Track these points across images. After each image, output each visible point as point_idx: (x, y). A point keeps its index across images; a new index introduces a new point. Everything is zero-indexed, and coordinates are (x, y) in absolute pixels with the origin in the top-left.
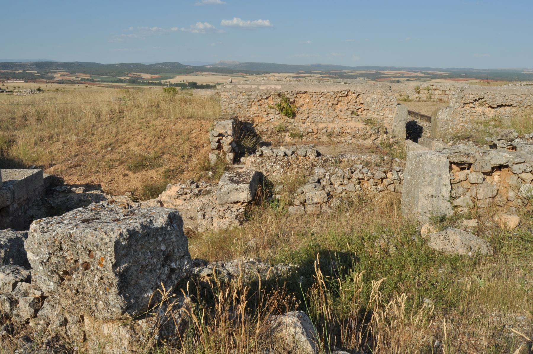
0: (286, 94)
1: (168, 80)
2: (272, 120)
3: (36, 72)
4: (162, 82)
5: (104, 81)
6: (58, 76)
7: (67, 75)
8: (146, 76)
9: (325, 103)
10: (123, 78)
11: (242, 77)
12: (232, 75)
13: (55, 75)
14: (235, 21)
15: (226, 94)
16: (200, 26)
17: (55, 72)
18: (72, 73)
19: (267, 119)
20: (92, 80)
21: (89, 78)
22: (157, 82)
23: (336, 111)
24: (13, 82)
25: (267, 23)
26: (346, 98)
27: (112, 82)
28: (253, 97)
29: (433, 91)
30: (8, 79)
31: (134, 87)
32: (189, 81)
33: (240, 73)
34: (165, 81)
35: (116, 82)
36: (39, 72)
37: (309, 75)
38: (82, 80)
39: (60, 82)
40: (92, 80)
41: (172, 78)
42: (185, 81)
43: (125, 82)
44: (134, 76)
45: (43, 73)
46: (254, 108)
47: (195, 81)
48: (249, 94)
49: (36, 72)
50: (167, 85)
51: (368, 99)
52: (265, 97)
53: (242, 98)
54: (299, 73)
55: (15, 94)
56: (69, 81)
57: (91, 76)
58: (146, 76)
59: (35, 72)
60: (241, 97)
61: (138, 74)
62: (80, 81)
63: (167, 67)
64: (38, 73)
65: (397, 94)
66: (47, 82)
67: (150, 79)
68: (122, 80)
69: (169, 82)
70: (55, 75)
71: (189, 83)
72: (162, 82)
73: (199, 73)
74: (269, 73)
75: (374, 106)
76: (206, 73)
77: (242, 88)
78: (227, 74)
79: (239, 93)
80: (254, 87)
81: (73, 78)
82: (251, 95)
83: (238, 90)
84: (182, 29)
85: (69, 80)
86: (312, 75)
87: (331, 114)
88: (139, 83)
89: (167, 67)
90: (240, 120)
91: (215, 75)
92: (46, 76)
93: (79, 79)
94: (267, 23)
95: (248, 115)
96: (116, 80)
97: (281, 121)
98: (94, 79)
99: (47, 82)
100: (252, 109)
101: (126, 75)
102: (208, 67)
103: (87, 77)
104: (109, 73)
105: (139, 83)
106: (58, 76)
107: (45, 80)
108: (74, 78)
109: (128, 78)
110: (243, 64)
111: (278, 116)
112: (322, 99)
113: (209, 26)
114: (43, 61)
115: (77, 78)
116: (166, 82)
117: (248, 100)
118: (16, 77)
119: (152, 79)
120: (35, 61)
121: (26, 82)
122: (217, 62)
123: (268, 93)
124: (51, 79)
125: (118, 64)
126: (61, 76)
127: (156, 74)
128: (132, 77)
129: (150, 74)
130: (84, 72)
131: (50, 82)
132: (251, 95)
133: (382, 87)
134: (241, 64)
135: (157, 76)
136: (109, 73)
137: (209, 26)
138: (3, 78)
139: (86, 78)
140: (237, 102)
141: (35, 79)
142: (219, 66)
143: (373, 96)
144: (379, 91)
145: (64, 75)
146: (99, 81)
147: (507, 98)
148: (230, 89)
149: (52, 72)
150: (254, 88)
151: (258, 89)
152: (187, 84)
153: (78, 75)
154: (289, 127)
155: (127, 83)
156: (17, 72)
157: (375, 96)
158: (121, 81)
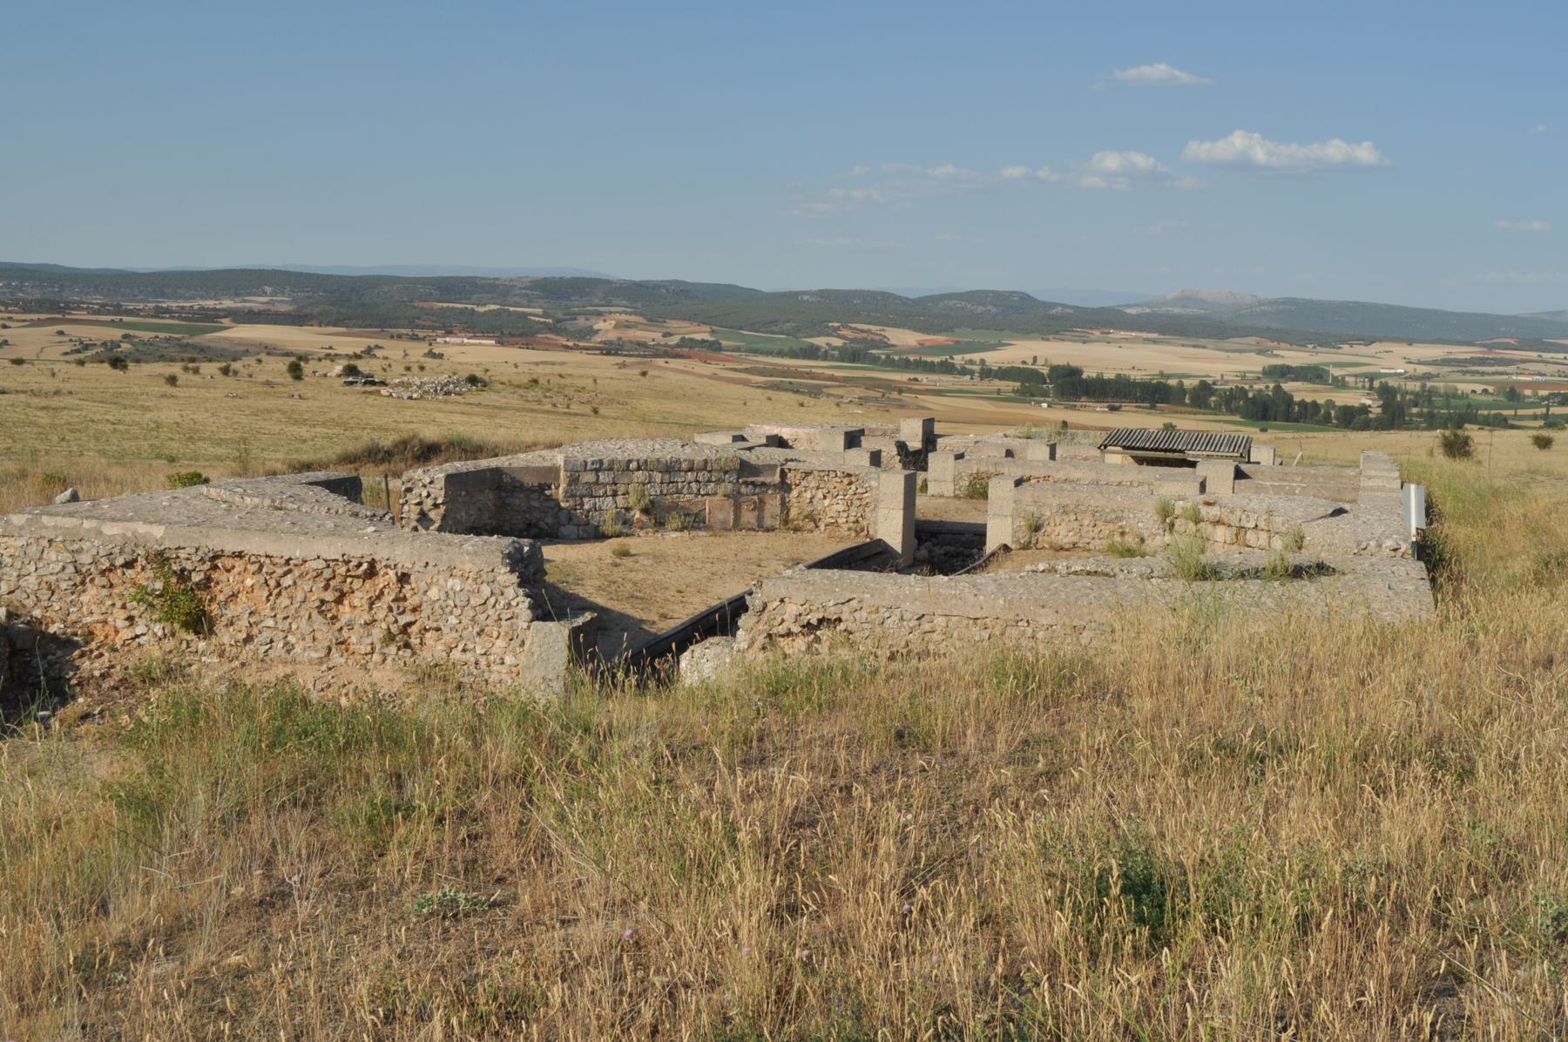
0: (182, 554)
1: (977, 357)
2: (142, 640)
3: (539, 311)
4: (958, 360)
5: (756, 352)
6: (606, 328)
7: (635, 326)
8: (904, 338)
9: (299, 597)
10: (820, 341)
11: (1259, 352)
12: (1226, 344)
13: (600, 325)
14: (1238, 140)
15: (11, 541)
16: (1112, 161)
17: (600, 314)
18: (653, 320)
19: (126, 634)
20: (714, 347)
21: (707, 337)
22: (936, 360)
23: (338, 625)
24: (462, 344)
25: (1365, 153)
26: (368, 583)
27: (780, 354)
28: (85, 559)
29: (1210, 528)
30: (449, 333)
31: (860, 374)
32: (1055, 363)
33: (1252, 340)
34: (968, 357)
35: (794, 355)
36: (552, 309)
37: (1534, 355)
38: (684, 343)
39: (609, 349)
40: (714, 347)
41: (993, 348)
42: (1040, 361)
43: (825, 357)
44: (859, 336)
45: (560, 316)
46: (91, 594)
47: (1074, 364)
48: (75, 547)
49: (539, 311)
50: (972, 373)
51: (434, 593)
52: (120, 561)
53: (55, 558)
54: (1491, 347)
55: (384, 391)
56: (643, 345)
57: (713, 332)
58: (904, 338)
59: (535, 312)
60: (53, 556)
61: (873, 328)
62: (677, 346)
63: (980, 309)
64: (545, 315)
65: (1111, 526)
66: (567, 347)
67: (913, 351)
68: (818, 348)
69: (983, 362)
70: (600, 325)
71: (1054, 369)
72: (958, 360)
73: (1097, 333)
74: (1369, 342)
75: (453, 620)
76: (1123, 334)
77: (55, 527)
78: (1203, 341)
79: (45, 543)
80: (87, 524)
81: (652, 336)
82: (80, 551)
83: (43, 532)
84: (1042, 173)
85: (639, 344)
86: (1546, 356)
87: (318, 635)
88: (875, 360)
89: (980, 309)
90: (52, 629)
91: (1154, 341)
92: (567, 325)
93: (675, 340)
94: (1365, 153)
95: (73, 617)
96: (796, 347)
97: (169, 644)
98: (724, 343)
99: (567, 347)
100: (85, 598)
101: (834, 332)
102: (1133, 311)
103: (702, 334)
104: (775, 322)
105: (875, 360)
106: (606, 328)
107: (563, 341)
108: (658, 336)
109: (838, 342)
110: (1270, 303)
111: (158, 629)
112: (287, 581)
113: (1141, 161)
114: (568, 275)
115: (666, 335)
116: (971, 362)
117: (71, 569)
118: (475, 326)
119: (923, 348)
120: (541, 275)
121: (501, 343)
122: (1172, 293)
123: (128, 549)
124: (582, 338)
125: (809, 293)
126: (616, 327)
127: (939, 332)
128: (852, 341)
129: (916, 329)
130: (693, 318)
131: (576, 348)
132: (80, 551)
133: (476, 553)
134: (1261, 304)
135: (941, 338)
136: (775, 322)
137: (1141, 161)
138: (433, 328)
139: (698, 337)
140: (41, 572)
141: (533, 334)
142: (1177, 310)
143: (450, 582)
144: (468, 567)
145: (628, 326)
146: (738, 349)
147: (927, 627)
148: (22, 528)
149: (588, 314)
150: (89, 530)
151: (99, 533)
152: (1045, 371)
153: (673, 324)
154: (194, 668)
155: (833, 358)
156: (481, 309)
157: (456, 584)
158: (812, 353)
